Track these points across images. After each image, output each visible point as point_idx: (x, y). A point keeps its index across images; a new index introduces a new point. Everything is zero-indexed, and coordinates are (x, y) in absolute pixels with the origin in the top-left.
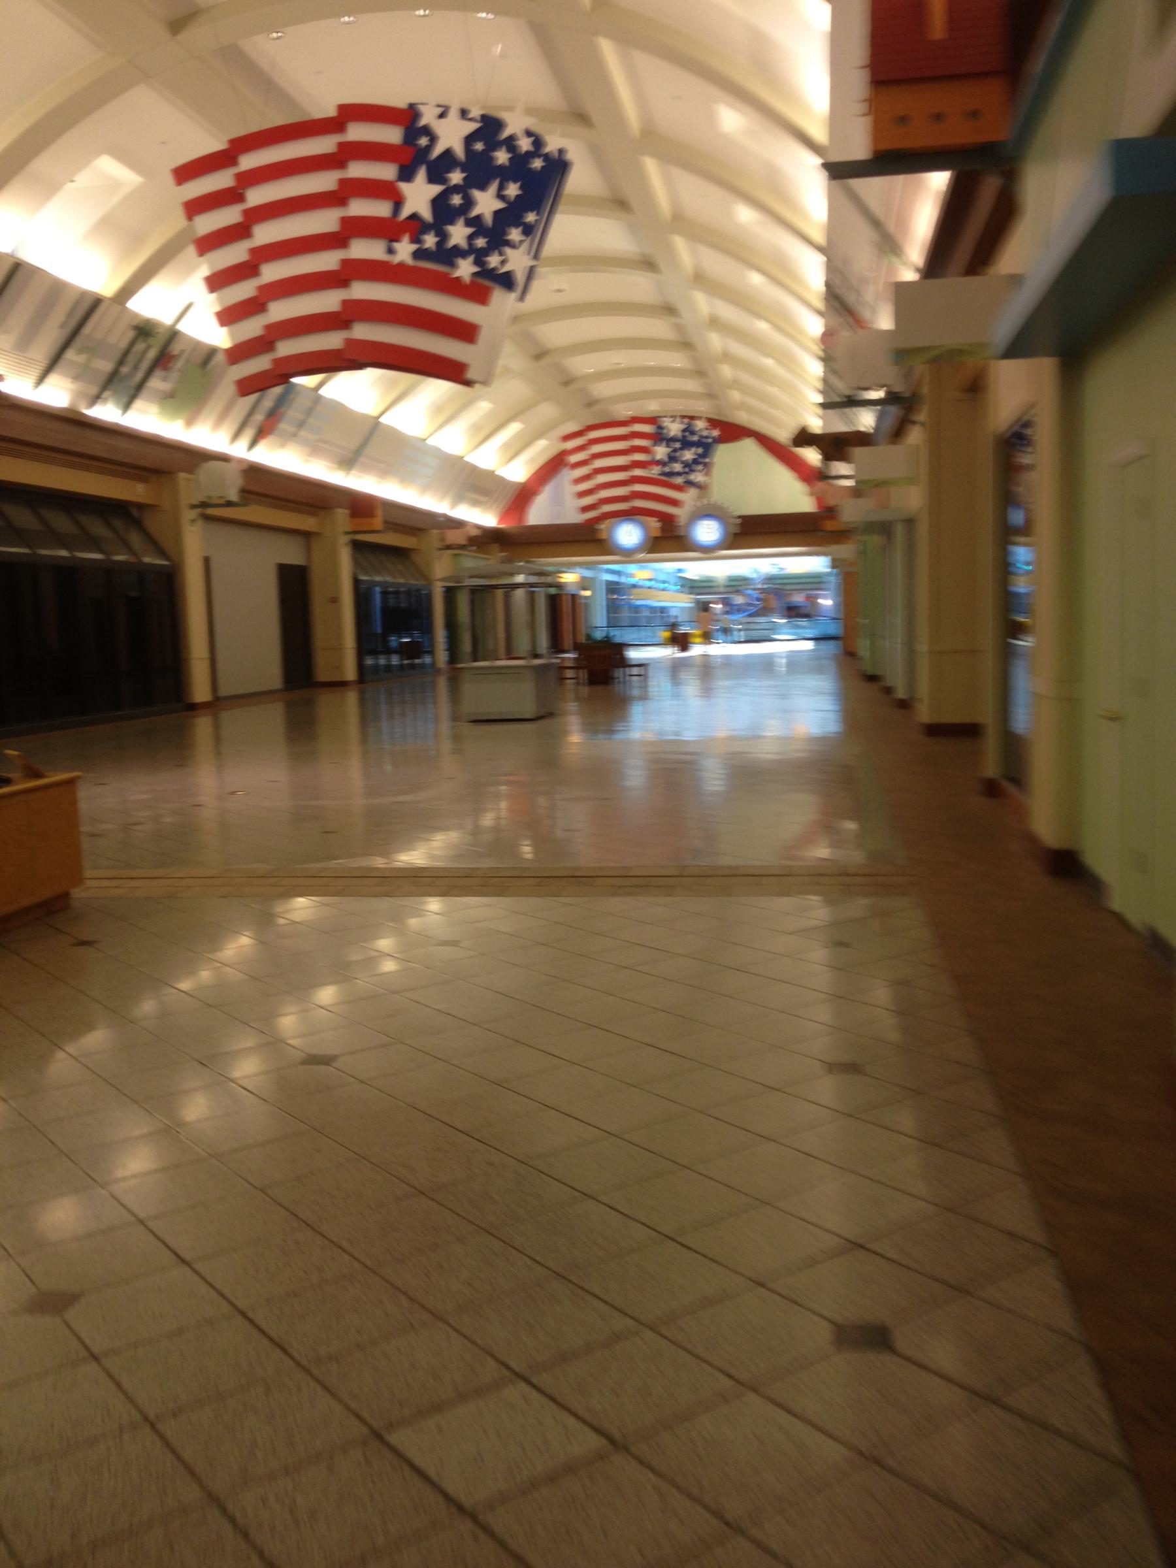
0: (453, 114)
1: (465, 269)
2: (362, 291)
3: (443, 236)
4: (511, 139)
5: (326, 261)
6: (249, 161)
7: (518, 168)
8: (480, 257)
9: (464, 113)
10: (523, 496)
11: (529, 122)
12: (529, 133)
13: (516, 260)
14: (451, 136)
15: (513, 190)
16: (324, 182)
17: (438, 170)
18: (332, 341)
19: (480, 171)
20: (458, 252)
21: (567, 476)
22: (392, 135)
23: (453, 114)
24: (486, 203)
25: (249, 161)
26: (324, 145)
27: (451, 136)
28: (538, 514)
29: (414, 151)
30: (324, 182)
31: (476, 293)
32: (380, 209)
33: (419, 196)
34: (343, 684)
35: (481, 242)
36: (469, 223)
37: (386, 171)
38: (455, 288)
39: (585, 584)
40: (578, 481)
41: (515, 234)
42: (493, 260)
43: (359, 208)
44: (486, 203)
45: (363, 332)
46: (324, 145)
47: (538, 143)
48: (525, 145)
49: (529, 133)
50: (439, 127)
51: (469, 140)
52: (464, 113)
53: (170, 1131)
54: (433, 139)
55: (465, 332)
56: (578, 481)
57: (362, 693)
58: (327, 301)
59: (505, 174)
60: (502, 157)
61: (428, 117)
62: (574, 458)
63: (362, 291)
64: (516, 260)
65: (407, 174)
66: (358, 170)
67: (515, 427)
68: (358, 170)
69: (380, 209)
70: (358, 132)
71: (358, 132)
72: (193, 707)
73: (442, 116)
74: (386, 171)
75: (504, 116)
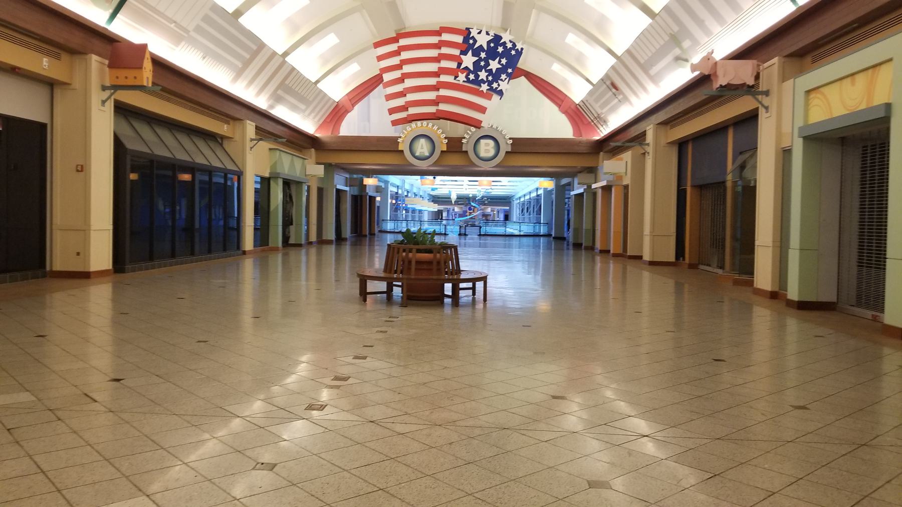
0: (484, 33)
1: (484, 87)
2: (443, 92)
3: (477, 76)
4: (505, 43)
5: (432, 81)
6: (403, 42)
7: (506, 53)
8: (490, 83)
9: (488, 33)
10: (338, 113)
11: (511, 38)
12: (511, 41)
13: (503, 85)
14: (482, 40)
15: (504, 61)
16: (433, 53)
17: (476, 53)
18: (431, 109)
19: (492, 54)
20: (483, 81)
21: (380, 92)
22: (459, 39)
23: (484, 33)
24: (494, 65)
25: (403, 42)
26: (434, 40)
27: (482, 40)
28: (350, 127)
29: (468, 44)
30: (433, 53)
31: (489, 98)
32: (454, 65)
33: (469, 60)
34: (300, 245)
35: (490, 78)
36: (486, 71)
37: (456, 52)
38: (480, 94)
39: (378, 189)
40: (389, 97)
41: (503, 76)
42: (495, 85)
43: (445, 64)
44: (494, 65)
45: (443, 107)
46: (434, 40)
47: (514, 45)
48: (509, 45)
49: (511, 41)
50: (477, 37)
51: (489, 43)
52: (488, 33)
53: (448, 296)
54: (475, 41)
55: (482, 110)
56: (389, 97)
57: (285, 255)
58: (431, 95)
59: (502, 56)
60: (500, 49)
61: (474, 33)
62: (387, 77)
63: (443, 92)
64: (503, 85)
65: (464, 53)
66: (445, 50)
67: (330, 40)
68: (445, 50)
69: (454, 65)
70: (446, 37)
71: (446, 37)
72: (244, 253)
73: (479, 33)
74: (456, 52)
75: (502, 35)
